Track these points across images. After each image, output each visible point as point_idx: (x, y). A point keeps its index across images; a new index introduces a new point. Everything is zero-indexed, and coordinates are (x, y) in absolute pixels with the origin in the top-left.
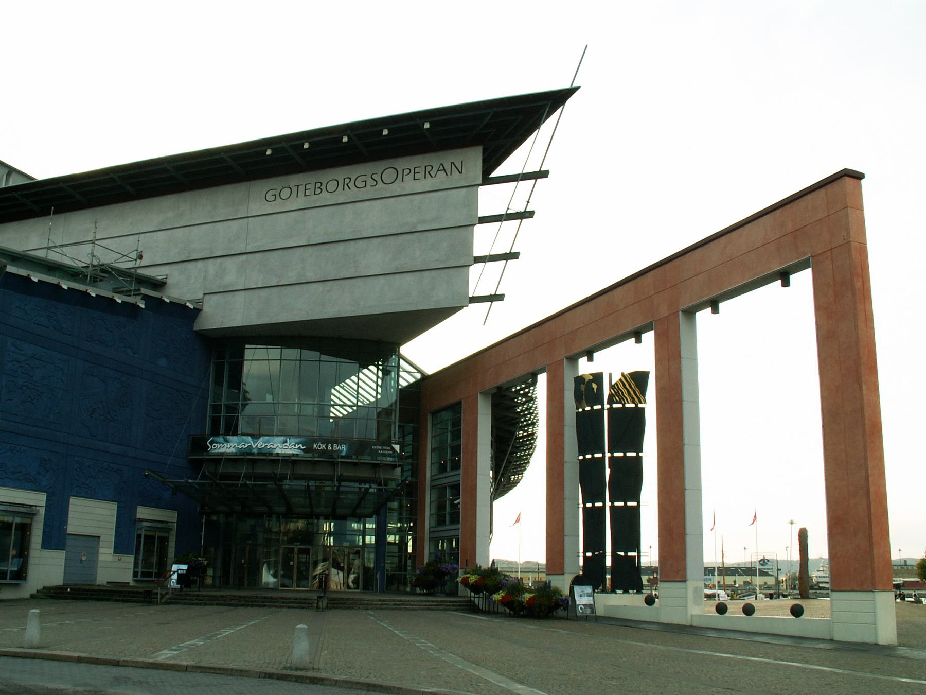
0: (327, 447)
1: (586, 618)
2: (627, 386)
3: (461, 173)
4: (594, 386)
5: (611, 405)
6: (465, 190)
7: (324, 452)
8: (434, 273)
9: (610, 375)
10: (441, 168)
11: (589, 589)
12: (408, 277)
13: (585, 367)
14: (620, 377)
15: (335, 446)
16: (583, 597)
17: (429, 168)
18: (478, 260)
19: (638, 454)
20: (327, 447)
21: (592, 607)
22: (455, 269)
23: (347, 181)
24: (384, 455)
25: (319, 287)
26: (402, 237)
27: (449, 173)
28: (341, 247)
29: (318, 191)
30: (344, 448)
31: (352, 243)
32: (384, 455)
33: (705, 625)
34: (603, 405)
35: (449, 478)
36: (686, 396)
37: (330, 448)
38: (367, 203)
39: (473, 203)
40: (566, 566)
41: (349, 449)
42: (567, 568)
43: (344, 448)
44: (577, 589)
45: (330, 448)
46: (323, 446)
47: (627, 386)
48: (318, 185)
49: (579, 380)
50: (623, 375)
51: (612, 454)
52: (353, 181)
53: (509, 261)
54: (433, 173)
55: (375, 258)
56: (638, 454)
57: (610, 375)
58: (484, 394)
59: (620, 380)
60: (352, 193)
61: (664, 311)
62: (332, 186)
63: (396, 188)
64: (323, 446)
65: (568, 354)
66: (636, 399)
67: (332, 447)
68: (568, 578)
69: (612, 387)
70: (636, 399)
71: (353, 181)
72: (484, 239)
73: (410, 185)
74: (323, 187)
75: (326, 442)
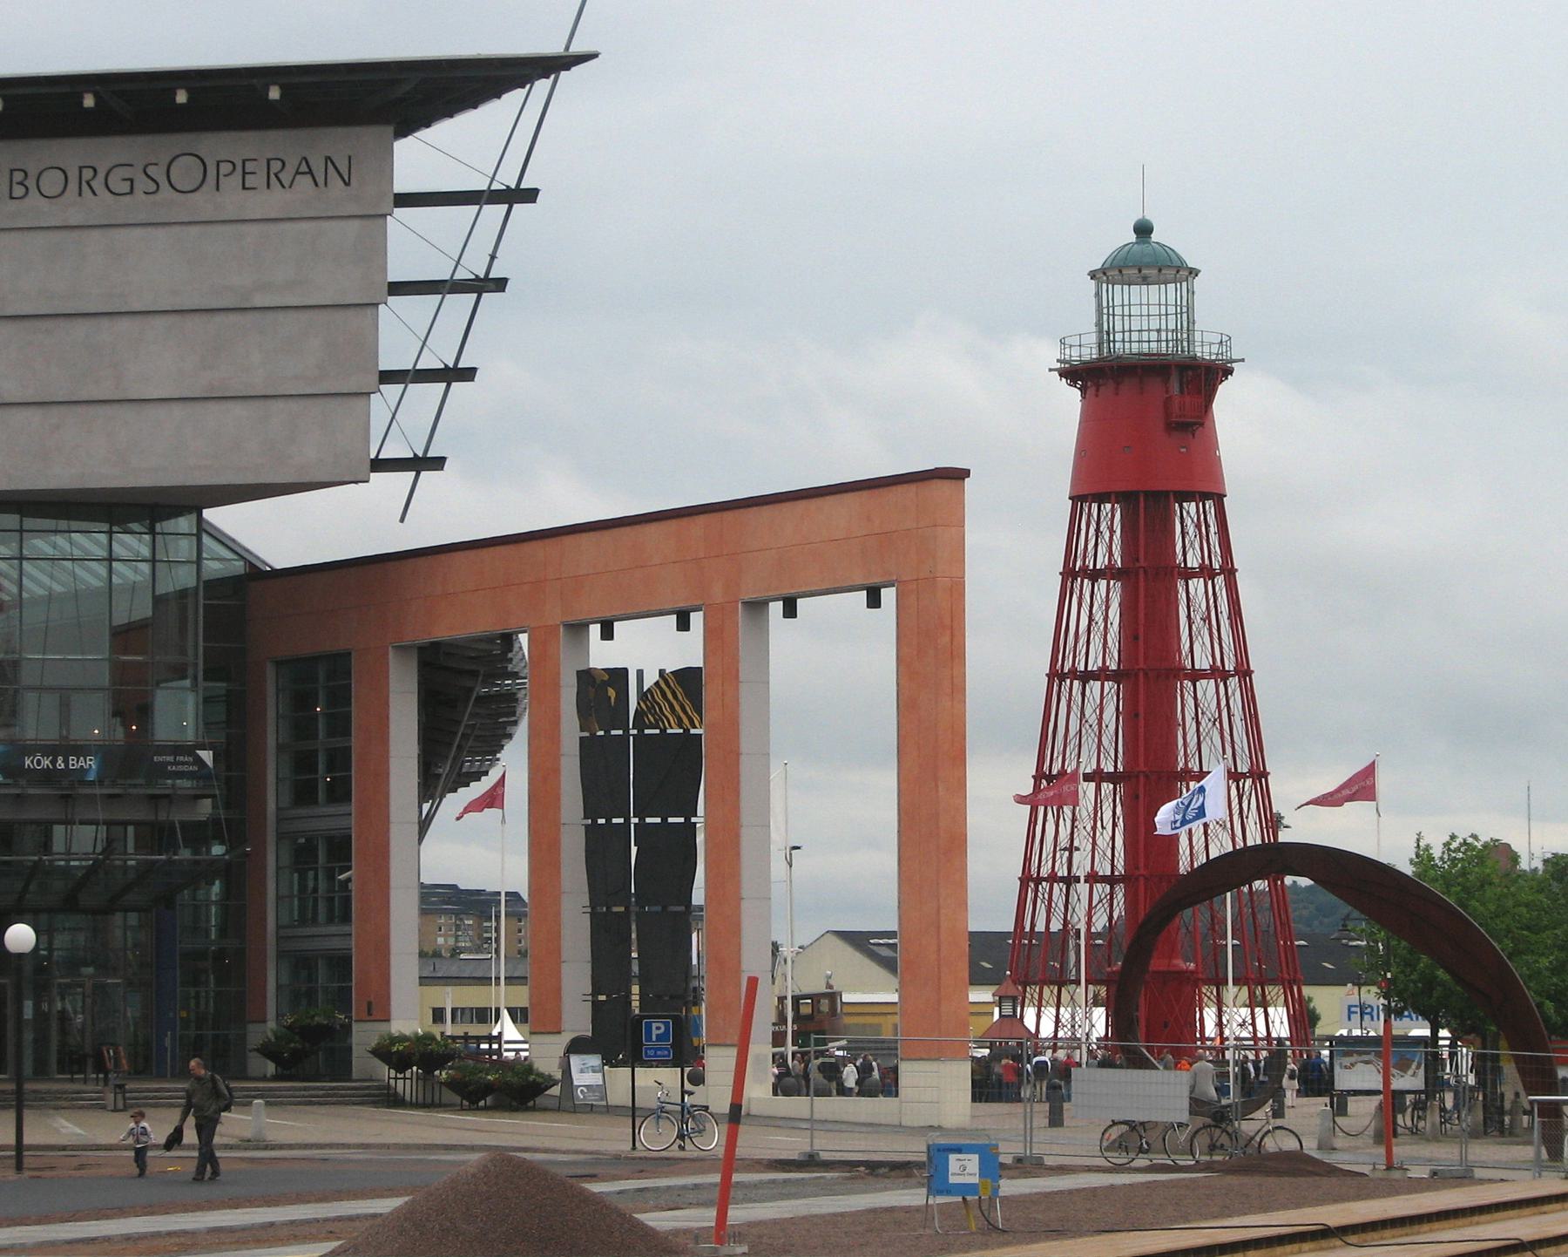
0: (54, 762)
1: (591, 1109)
2: (670, 696)
3: (347, 184)
4: (612, 693)
5: (641, 731)
6: (356, 223)
7: (48, 777)
8: (294, 406)
9: (640, 673)
10: (304, 168)
11: (595, 1060)
12: (238, 409)
13: (601, 654)
14: (656, 677)
15: (72, 760)
16: (586, 1073)
17: (276, 166)
18: (388, 377)
19: (687, 819)
20: (54, 762)
21: (602, 1090)
22: (339, 399)
23: (88, 174)
24: (181, 775)
25: (34, 416)
26: (219, 318)
27: (321, 180)
28: (80, 329)
29: (18, 191)
30: (91, 763)
31: (105, 322)
32: (181, 775)
33: (766, 1114)
34: (626, 730)
35: (322, 819)
36: (746, 744)
37: (60, 764)
38: (138, 232)
39: (377, 250)
40: (564, 1017)
41: (104, 765)
42: (565, 1025)
43: (91, 763)
44: (576, 1061)
45: (60, 764)
46: (46, 762)
47: (670, 696)
48: (18, 176)
49: (587, 677)
50: (662, 672)
51: (642, 819)
52: (101, 176)
53: (454, 385)
54: (286, 177)
55: (159, 361)
56: (687, 819)
57: (640, 673)
58: (402, 649)
59: (657, 684)
60: (99, 205)
61: (718, 594)
62: (52, 182)
63: (203, 204)
64: (46, 762)
65: (570, 619)
66: (686, 721)
67: (66, 762)
68: (561, 1042)
69: (643, 696)
70: (686, 721)
71: (101, 176)
72: (401, 332)
73: (231, 199)
74: (31, 183)
75: (52, 751)
